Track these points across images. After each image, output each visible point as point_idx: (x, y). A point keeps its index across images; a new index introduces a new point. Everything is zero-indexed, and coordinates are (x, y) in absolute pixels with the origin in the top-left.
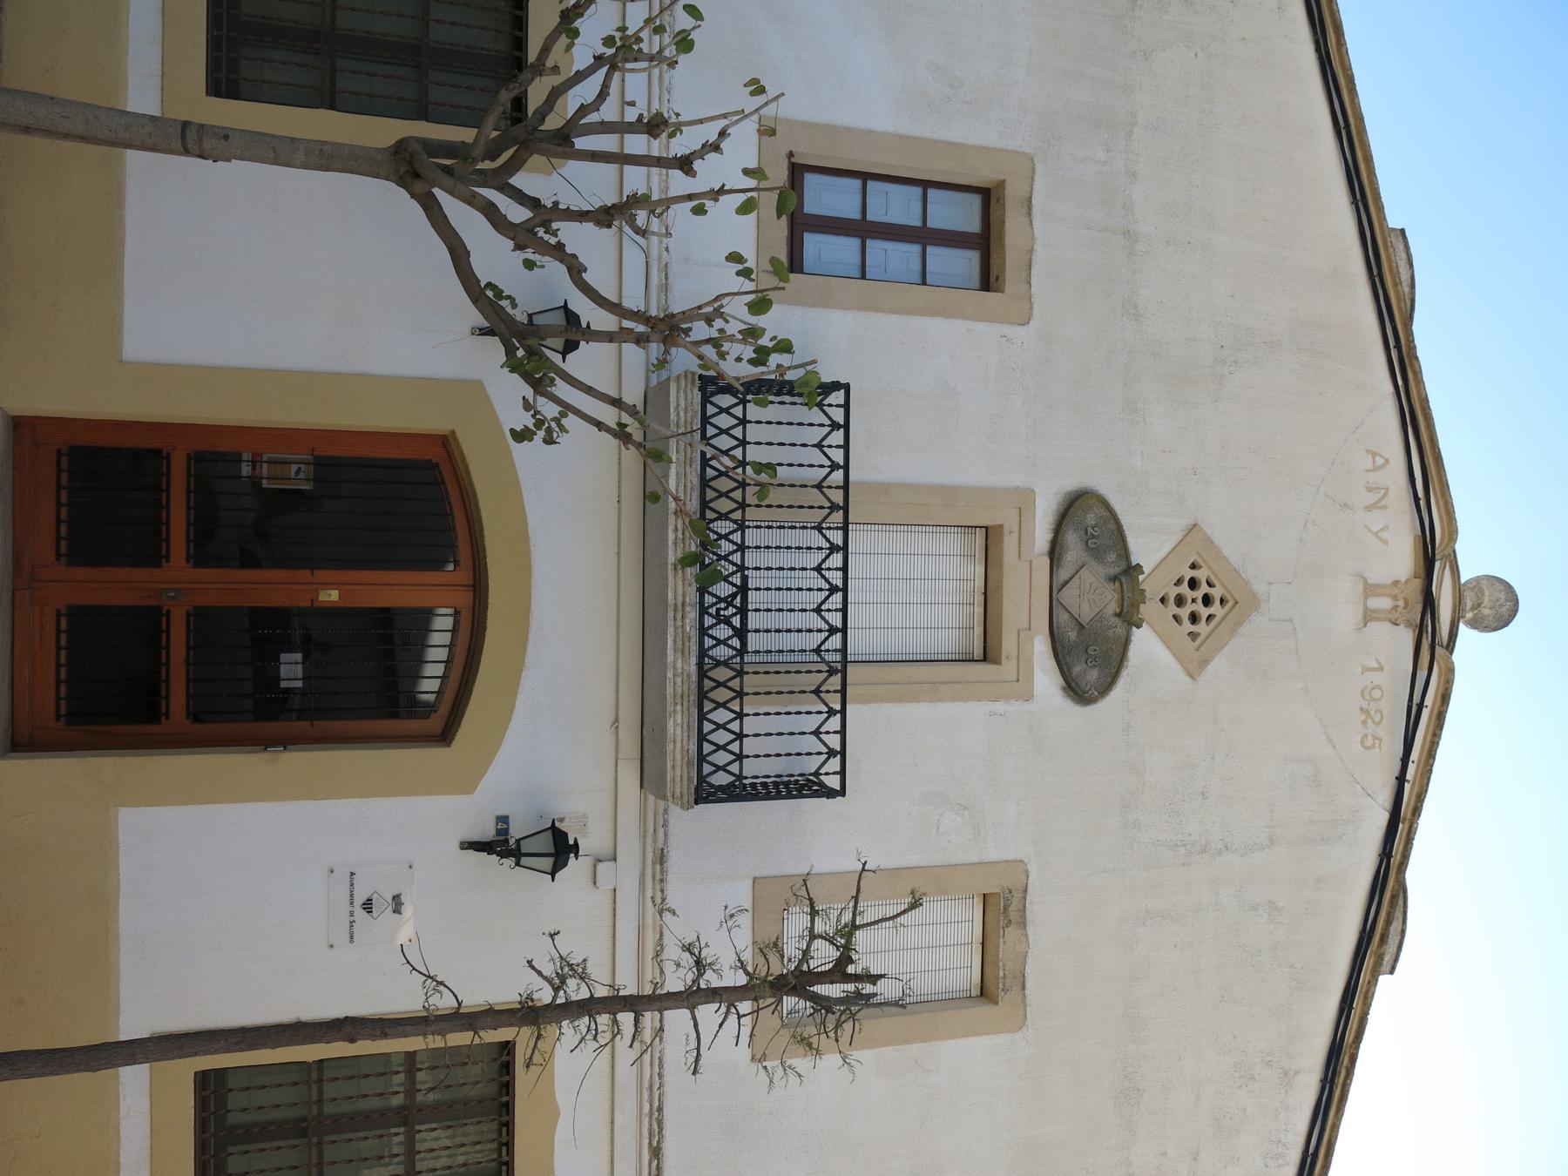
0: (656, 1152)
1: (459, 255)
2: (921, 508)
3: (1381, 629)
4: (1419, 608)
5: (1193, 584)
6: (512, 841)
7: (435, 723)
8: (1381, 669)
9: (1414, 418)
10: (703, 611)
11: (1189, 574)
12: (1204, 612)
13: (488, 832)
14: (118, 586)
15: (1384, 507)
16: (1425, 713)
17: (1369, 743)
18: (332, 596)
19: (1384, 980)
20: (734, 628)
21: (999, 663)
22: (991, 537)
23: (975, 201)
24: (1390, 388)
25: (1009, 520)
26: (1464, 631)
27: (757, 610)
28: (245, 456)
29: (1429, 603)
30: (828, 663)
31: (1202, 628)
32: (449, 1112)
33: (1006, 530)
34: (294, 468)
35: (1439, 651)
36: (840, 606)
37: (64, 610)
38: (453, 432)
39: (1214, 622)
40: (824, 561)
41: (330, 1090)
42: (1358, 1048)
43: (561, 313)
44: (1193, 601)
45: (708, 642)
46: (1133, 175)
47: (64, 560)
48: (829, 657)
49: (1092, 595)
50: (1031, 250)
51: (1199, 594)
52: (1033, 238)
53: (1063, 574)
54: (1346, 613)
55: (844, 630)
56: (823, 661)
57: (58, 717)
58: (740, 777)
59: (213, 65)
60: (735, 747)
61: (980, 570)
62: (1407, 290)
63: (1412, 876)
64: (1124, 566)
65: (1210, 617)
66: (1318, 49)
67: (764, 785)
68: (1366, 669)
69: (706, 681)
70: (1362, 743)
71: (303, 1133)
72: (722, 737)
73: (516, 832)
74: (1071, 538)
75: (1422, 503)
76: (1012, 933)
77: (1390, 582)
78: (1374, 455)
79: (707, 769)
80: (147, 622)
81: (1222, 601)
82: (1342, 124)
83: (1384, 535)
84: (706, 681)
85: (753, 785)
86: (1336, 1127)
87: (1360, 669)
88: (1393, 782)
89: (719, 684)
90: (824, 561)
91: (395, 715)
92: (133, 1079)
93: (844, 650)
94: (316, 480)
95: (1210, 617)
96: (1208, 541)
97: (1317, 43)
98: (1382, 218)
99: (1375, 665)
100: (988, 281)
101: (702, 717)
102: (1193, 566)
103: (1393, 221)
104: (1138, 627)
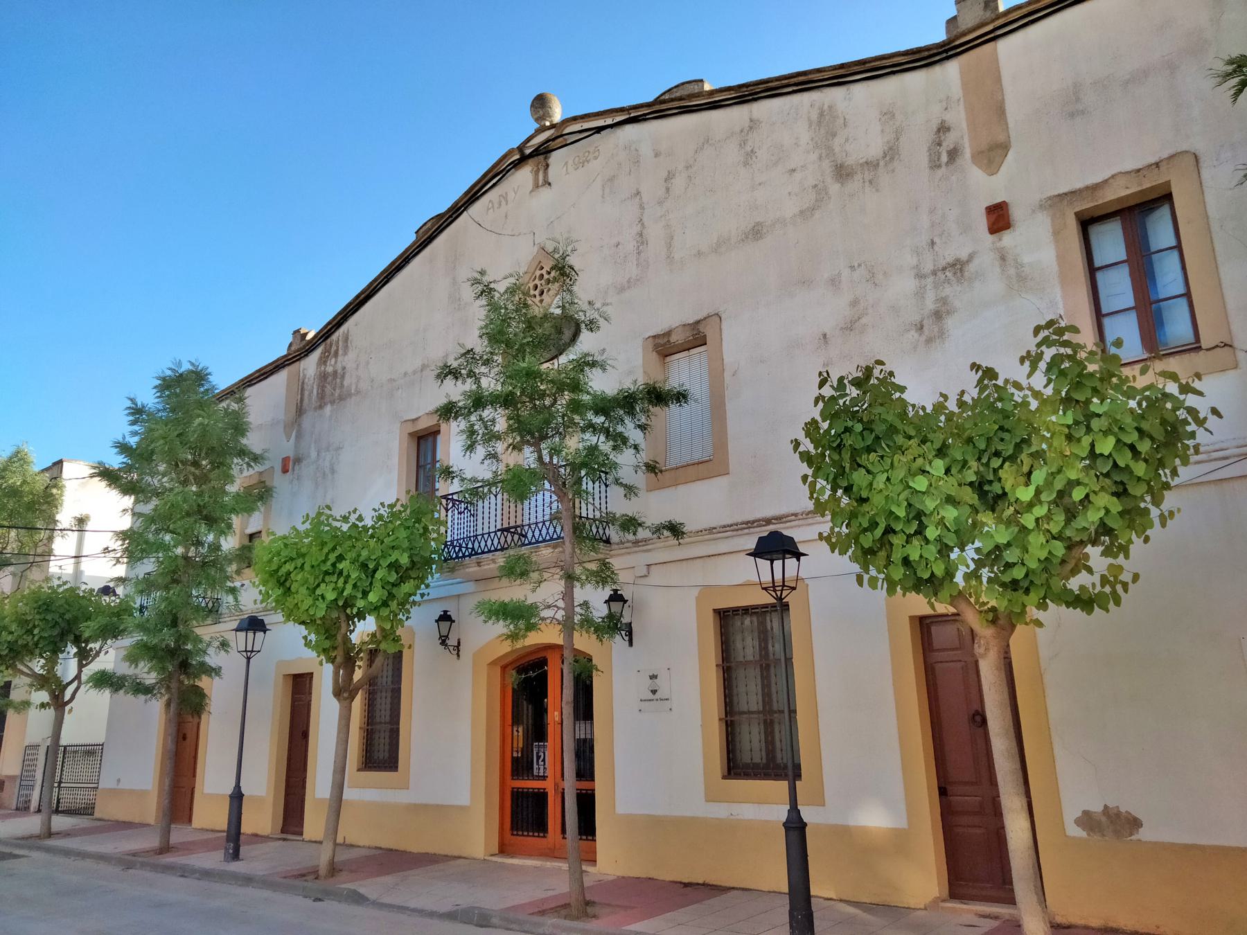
0: (711, 530)
23: (1096, 232)
46: (406, 374)
76: (673, 338)
92: (349, 794)
98: (414, 243)
103: (413, 238)
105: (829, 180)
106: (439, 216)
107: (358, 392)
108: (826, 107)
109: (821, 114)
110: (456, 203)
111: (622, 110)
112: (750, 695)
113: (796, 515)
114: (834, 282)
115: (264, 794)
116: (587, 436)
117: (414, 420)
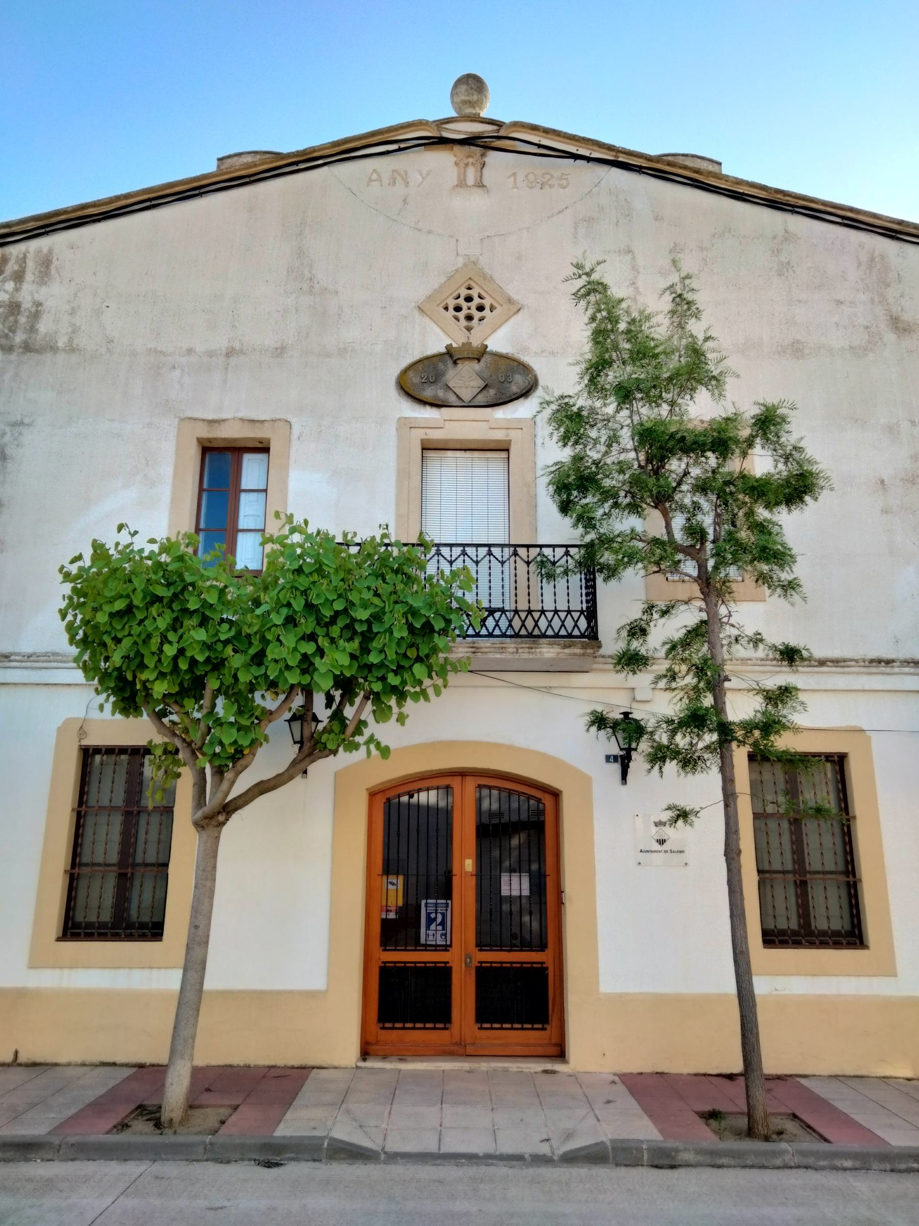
1: (262, 788)
2: (415, 495)
3: (489, 175)
4: (473, 148)
5: (458, 309)
6: (621, 753)
7: (548, 800)
8: (514, 174)
9: (345, 151)
10: (477, 635)
11: (451, 311)
12: (477, 301)
13: (616, 768)
14: (463, 995)
15: (406, 172)
16: (545, 142)
17: (564, 183)
18: (469, 865)
19: (726, 170)
20: (488, 616)
21: (510, 441)
22: (427, 447)
24: (326, 168)
25: (418, 436)
26: (485, 114)
27: (490, 601)
28: (384, 916)
29: (470, 141)
30: (510, 556)
31: (487, 303)
32: (792, 791)
33: (425, 437)
34: (390, 887)
35: (502, 133)
36: (474, 549)
37: (479, 1025)
38: (367, 789)
39: (483, 294)
40: (445, 559)
41: (777, 866)
42: (770, 188)
43: (293, 724)
44: (469, 309)
45: (497, 632)
46: (190, 351)
47: (448, 1025)
48: (506, 556)
49: (465, 379)
50: (242, 420)
51: (465, 305)
52: (234, 419)
53: (452, 399)
54: (477, 201)
55: (489, 546)
56: (509, 559)
57: (544, 1029)
58: (582, 612)
59: (143, 938)
60: (562, 615)
61: (450, 454)
62: (258, 157)
63: (653, 151)
64: (447, 357)
65: (480, 297)
66: (99, 221)
67: (587, 594)
68: (515, 186)
69: (521, 633)
70: (564, 188)
71: (804, 883)
72: (556, 623)
73: (616, 751)
74: (428, 393)
75: (402, 146)
77: (456, 169)
78: (370, 180)
79: (576, 632)
80: (486, 977)
81: (469, 288)
82: (148, 204)
83: (424, 172)
84: (521, 633)
85: (587, 602)
86: (825, 203)
87: (515, 190)
88: (591, 164)
89: (523, 625)
90: (445, 559)
91: (543, 823)
92: (761, 986)
93: (502, 546)
94: (397, 874)
95: (480, 297)
96: (429, 298)
97: (94, 221)
99: (512, 179)
100: (263, 449)
101: (544, 636)
102: (446, 309)
104: (486, 347)
105: (883, 327)
106: (278, 155)
107: (72, 349)
108: (877, 254)
109: (872, 259)
110: (314, 149)
111: (610, 148)
112: (106, 841)
113: (856, 661)
114: (892, 430)
115: (316, 980)
116: (738, 523)
117: (211, 422)
